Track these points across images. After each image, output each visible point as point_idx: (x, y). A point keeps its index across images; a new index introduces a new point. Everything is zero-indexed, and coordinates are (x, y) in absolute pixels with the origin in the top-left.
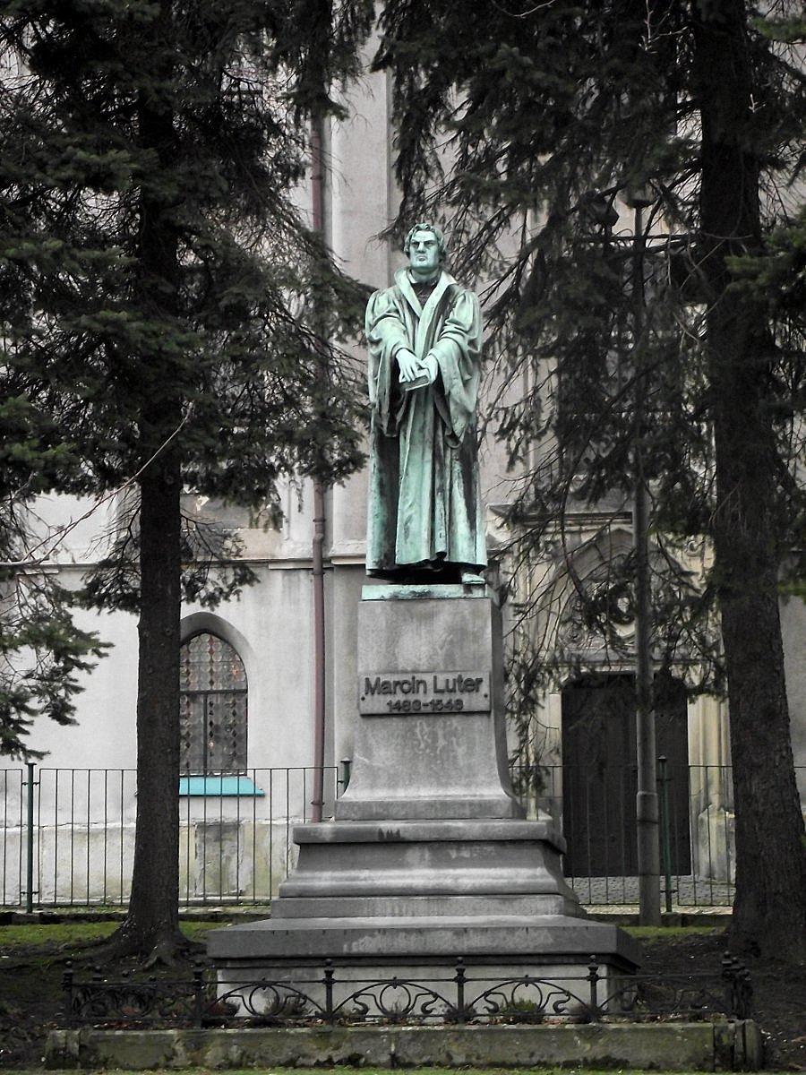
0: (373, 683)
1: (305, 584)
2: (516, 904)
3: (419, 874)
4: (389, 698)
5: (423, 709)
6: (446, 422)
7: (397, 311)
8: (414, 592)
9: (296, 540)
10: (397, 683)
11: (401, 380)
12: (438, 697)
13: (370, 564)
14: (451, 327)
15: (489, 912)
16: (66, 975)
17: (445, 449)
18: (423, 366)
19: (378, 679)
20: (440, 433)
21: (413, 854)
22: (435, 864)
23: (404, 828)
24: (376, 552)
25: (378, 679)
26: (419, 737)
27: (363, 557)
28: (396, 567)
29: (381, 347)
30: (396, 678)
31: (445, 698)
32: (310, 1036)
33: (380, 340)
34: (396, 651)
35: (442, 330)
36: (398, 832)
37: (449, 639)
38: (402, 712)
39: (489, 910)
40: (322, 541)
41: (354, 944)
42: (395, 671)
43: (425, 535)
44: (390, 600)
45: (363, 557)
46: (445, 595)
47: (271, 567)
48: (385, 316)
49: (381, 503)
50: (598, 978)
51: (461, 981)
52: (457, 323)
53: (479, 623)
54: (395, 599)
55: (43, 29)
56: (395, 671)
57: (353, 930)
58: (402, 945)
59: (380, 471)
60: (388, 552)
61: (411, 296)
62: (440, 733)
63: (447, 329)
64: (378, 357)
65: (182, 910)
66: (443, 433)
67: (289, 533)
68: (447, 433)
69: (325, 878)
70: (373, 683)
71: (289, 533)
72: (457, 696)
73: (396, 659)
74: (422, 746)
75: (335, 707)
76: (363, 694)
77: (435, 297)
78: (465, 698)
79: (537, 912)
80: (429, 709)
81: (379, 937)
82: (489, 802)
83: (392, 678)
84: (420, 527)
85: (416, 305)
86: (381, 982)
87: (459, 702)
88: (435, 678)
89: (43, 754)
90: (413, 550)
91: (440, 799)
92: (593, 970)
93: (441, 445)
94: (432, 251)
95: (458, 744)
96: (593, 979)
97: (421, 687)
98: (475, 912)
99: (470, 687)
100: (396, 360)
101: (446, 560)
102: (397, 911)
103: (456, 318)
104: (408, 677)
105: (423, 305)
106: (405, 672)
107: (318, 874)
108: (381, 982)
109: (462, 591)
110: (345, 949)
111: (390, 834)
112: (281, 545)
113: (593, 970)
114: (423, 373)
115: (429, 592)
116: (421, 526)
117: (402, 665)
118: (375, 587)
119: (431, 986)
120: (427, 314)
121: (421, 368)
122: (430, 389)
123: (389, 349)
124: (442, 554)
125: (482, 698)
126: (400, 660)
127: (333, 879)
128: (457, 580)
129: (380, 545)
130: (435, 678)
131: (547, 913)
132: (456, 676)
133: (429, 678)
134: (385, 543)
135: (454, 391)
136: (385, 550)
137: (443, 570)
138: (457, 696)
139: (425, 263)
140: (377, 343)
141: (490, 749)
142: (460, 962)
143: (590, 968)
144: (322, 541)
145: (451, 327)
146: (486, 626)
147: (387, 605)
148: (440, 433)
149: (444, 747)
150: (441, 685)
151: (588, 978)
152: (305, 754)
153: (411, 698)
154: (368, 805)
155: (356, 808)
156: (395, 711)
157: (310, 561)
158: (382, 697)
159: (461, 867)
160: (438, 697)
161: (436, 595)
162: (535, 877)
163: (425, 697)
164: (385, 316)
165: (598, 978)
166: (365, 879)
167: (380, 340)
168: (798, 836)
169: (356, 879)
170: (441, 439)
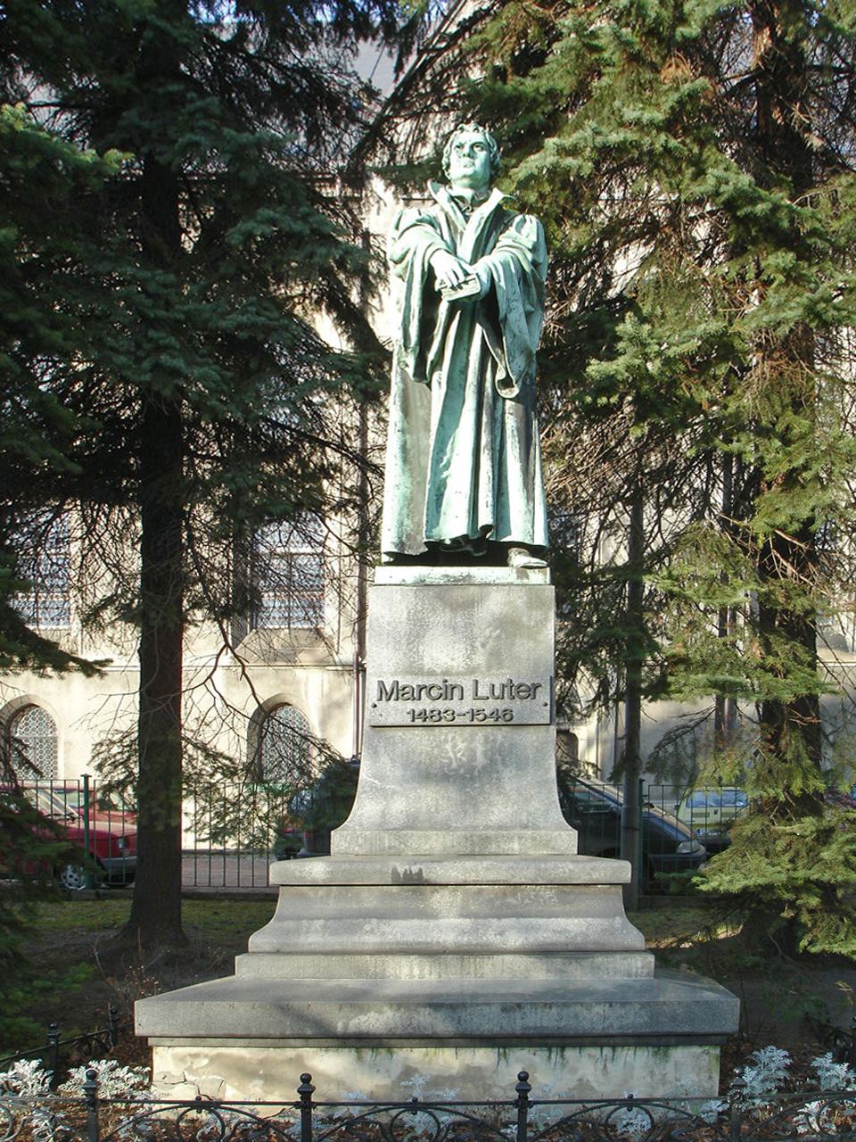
4: (410, 705)
10: (421, 688)
18: (469, 272)
20: (489, 375)
26: (451, 754)
34: (421, 647)
37: (494, 634)
42: (420, 672)
44: (414, 585)
48: (415, 225)
49: (403, 471)
54: (422, 584)
55: (438, 42)
75: (218, 980)
78: (516, 705)
83: (415, 682)
89: (455, 253)
90: (453, 526)
97: (456, 692)
100: (431, 268)
104: (438, 681)
106: (431, 673)
109: (515, 575)
115: (469, 576)
117: (427, 663)
122: (478, 304)
124: (487, 528)
133: (467, 684)
135: (512, 317)
146: (546, 619)
147: (410, 592)
156: (419, 722)
158: (400, 703)
160: (479, 704)
168: (647, 258)
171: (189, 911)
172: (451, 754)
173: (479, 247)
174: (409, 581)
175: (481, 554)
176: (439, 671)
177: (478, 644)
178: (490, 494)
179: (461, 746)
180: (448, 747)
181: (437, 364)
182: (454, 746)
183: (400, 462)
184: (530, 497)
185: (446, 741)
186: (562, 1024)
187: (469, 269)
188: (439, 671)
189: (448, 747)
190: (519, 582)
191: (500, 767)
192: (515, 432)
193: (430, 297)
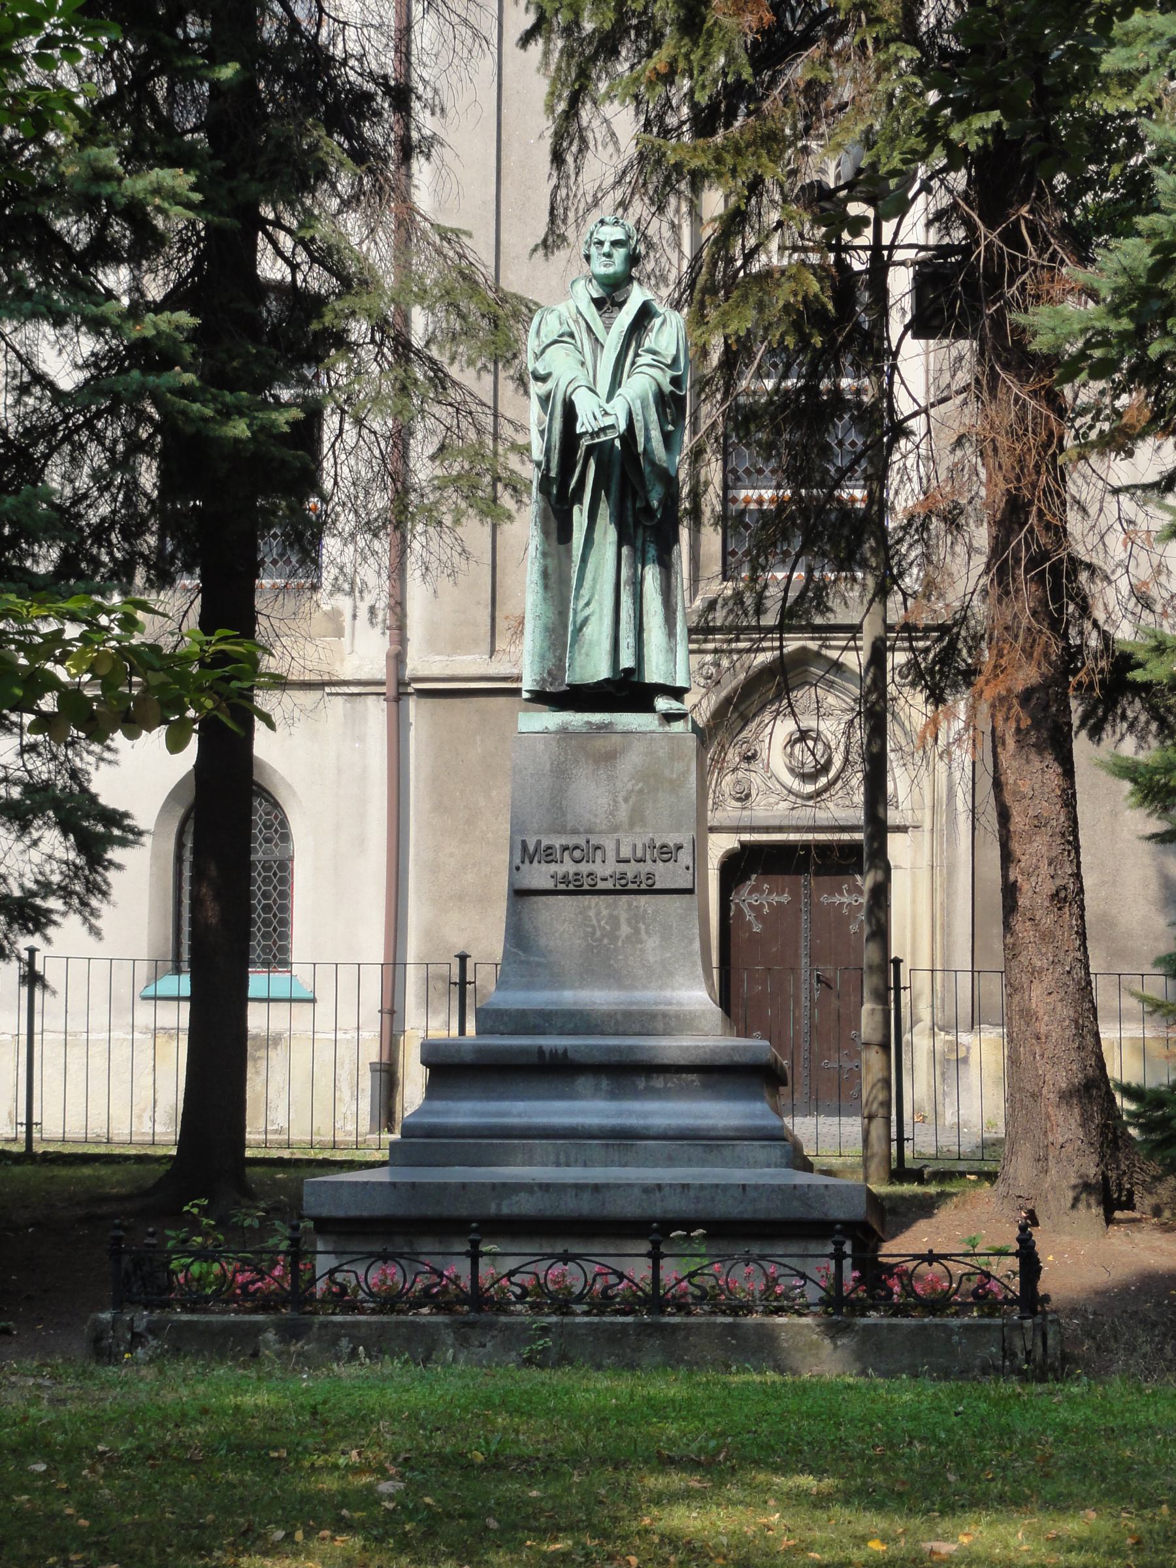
0: (531, 848)
1: (376, 712)
2: (727, 1152)
3: (591, 1109)
4: (553, 868)
5: (601, 885)
6: (638, 488)
7: (572, 335)
8: (589, 723)
9: (364, 654)
10: (565, 848)
11: (579, 430)
12: (623, 867)
13: (528, 684)
14: (646, 358)
15: (689, 1163)
16: (114, 1238)
17: (636, 526)
19: (539, 842)
20: (629, 504)
21: (583, 1083)
22: (613, 1095)
23: (573, 1046)
24: (536, 668)
25: (539, 842)
26: (594, 922)
27: (519, 679)
28: (564, 688)
29: (550, 385)
30: (571, 841)
31: (631, 869)
32: (447, 1326)
33: (549, 375)
35: (633, 363)
36: (565, 1051)
38: (571, 887)
39: (690, 1160)
40: (398, 659)
41: (505, 1203)
43: (606, 644)
44: (556, 732)
45: (519, 679)
46: (633, 727)
47: (327, 690)
48: (555, 342)
49: (545, 599)
50: (845, 1256)
51: (475, 1256)
52: (654, 353)
53: (679, 767)
54: (564, 732)
56: (562, 830)
57: (504, 1185)
58: (569, 1206)
59: (544, 555)
60: (556, 670)
61: (591, 313)
62: (623, 917)
63: (640, 361)
64: (545, 400)
65: (249, 1153)
66: (634, 504)
67: (352, 644)
68: (638, 505)
69: (466, 1111)
70: (531, 848)
71: (352, 644)
72: (648, 867)
73: (564, 814)
74: (598, 934)
76: (518, 861)
77: (625, 317)
79: (756, 1164)
80: (609, 885)
81: (539, 1194)
82: (690, 1012)
83: (558, 842)
84: (600, 633)
85: (597, 325)
86: (550, 1256)
87: (650, 876)
88: (618, 841)
90: (594, 667)
91: (623, 1007)
92: (839, 1245)
93: (630, 520)
94: (620, 254)
95: (647, 933)
96: (839, 1257)
98: (671, 1161)
99: (665, 856)
101: (635, 679)
102: (562, 1159)
103: (654, 346)
105: (608, 328)
107: (451, 1105)
108: (550, 1256)
110: (493, 1209)
111: (554, 1053)
112: (342, 660)
113: (839, 1245)
114: (608, 421)
115: (611, 723)
116: (598, 632)
118: (535, 714)
119: (611, 1262)
120: (613, 341)
121: (606, 414)
123: (562, 388)
124: (629, 671)
125: (681, 871)
126: (569, 817)
127: (475, 1113)
128: (651, 709)
129: (543, 657)
130: (618, 841)
131: (769, 1166)
132: (647, 841)
134: (549, 655)
136: (550, 664)
137: (628, 691)
138: (648, 867)
139: (611, 270)
140: (543, 379)
141: (691, 941)
142: (475, 1231)
143: (835, 1243)
144: (398, 659)
145: (646, 358)
148: (629, 504)
149: (628, 937)
150: (626, 852)
151: (648, 1255)
152: (372, 946)
153: (584, 868)
154: (523, 1013)
155: (506, 1019)
156: (562, 887)
157: (380, 683)
158: (544, 867)
159: (652, 1099)
161: (619, 728)
162: (753, 1116)
163: (604, 869)
164: (555, 342)
165: (845, 1256)
166: (519, 1115)
167: (549, 375)
169: (630, 1113)
170: (630, 513)
171: (249, 1171)
172: (594, 922)
173: (616, 1138)
174: (552, 728)
176: (921, 627)
177: (620, 799)
178: (632, 635)
179: (605, 912)
180: (592, 913)
181: (578, 496)
182: (598, 914)
183: (539, 589)
184: (671, 633)
185: (589, 907)
186: (700, 1206)
187: (608, 407)
188: (921, 627)
189: (592, 913)
190: (661, 729)
191: (644, 936)
193: (570, 437)
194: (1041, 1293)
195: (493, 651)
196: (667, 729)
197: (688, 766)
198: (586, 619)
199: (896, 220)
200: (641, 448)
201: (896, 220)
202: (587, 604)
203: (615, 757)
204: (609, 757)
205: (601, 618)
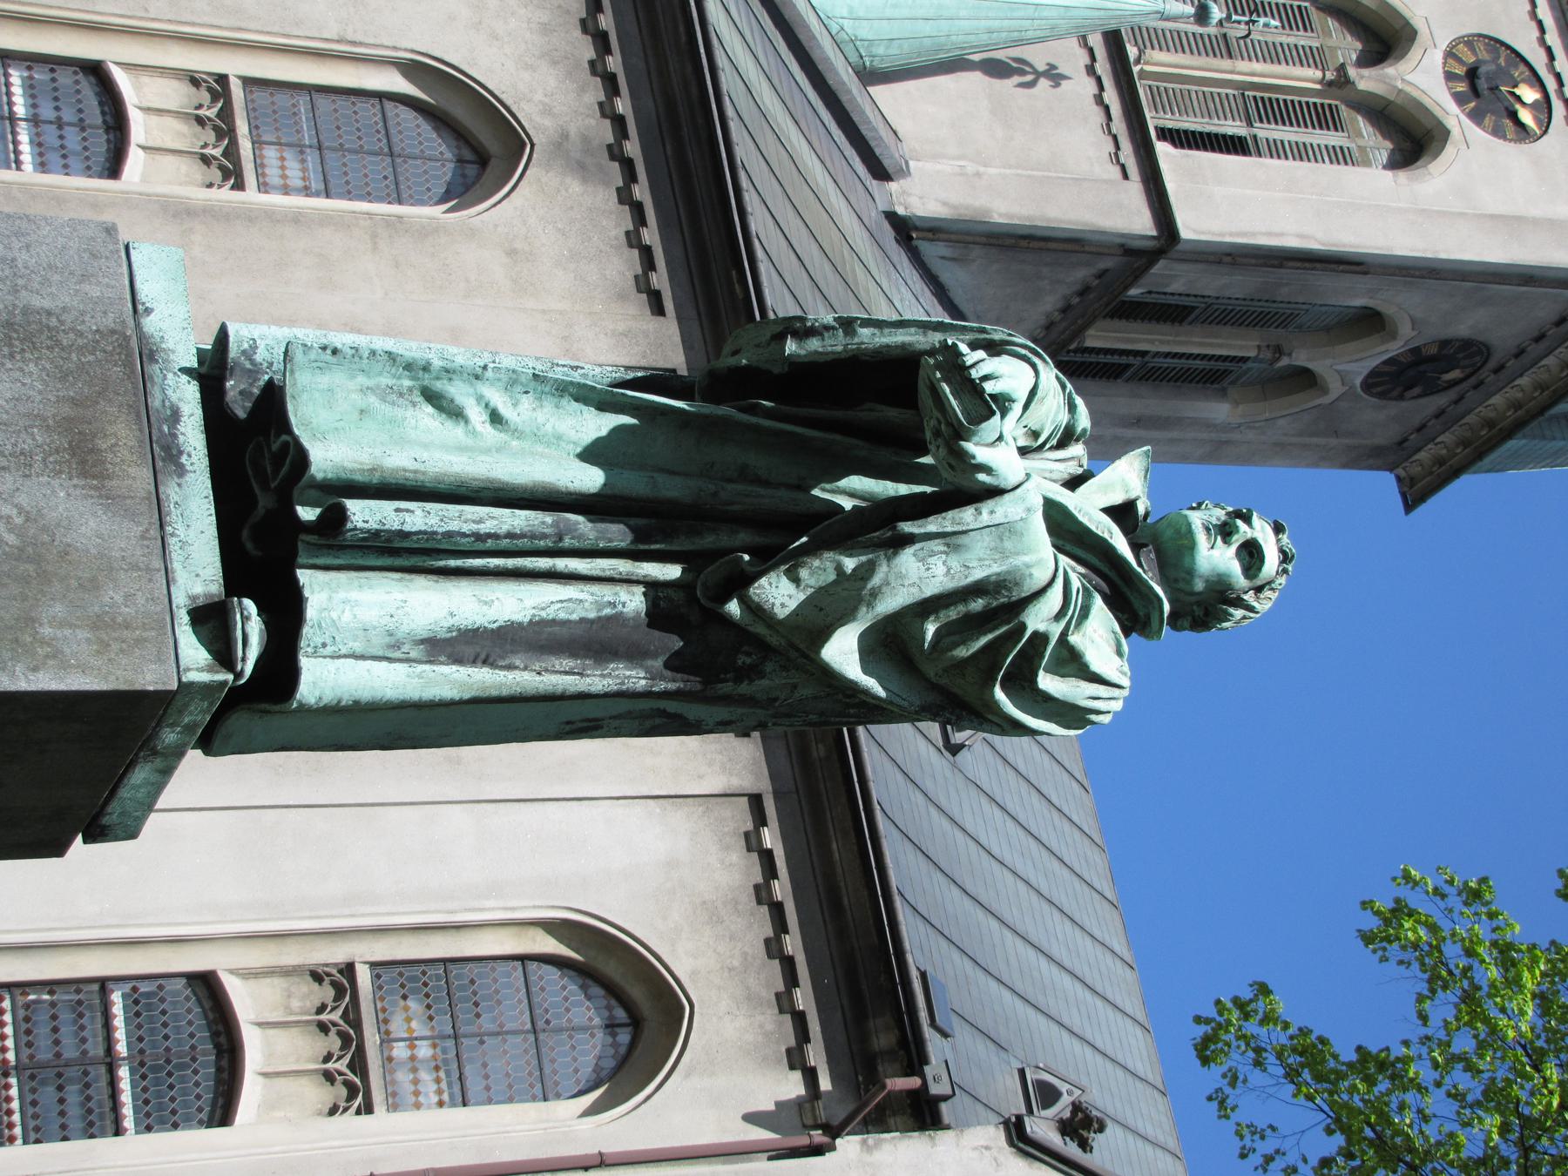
8: (175, 416)
20: (744, 537)
43: (399, 460)
44: (142, 336)
109: (199, 589)
115: (181, 471)
161: (171, 491)
174: (150, 324)
175: (249, 546)
190: (180, 599)
192: (608, 611)
194: (773, 1108)
195: (265, 1075)
196: (183, 618)
197: (84, 669)
198: (454, 413)
199: (1172, 1143)
200: (907, 527)
201: (1172, 1143)
202: (496, 418)
203: (84, 474)
204: (83, 458)
205: (461, 449)
